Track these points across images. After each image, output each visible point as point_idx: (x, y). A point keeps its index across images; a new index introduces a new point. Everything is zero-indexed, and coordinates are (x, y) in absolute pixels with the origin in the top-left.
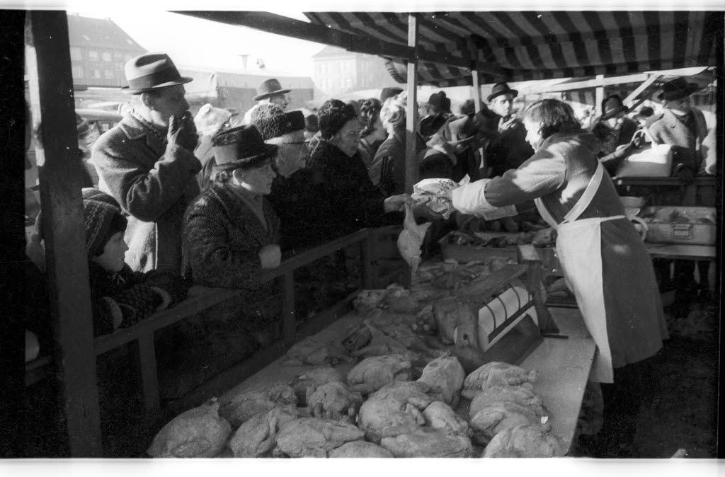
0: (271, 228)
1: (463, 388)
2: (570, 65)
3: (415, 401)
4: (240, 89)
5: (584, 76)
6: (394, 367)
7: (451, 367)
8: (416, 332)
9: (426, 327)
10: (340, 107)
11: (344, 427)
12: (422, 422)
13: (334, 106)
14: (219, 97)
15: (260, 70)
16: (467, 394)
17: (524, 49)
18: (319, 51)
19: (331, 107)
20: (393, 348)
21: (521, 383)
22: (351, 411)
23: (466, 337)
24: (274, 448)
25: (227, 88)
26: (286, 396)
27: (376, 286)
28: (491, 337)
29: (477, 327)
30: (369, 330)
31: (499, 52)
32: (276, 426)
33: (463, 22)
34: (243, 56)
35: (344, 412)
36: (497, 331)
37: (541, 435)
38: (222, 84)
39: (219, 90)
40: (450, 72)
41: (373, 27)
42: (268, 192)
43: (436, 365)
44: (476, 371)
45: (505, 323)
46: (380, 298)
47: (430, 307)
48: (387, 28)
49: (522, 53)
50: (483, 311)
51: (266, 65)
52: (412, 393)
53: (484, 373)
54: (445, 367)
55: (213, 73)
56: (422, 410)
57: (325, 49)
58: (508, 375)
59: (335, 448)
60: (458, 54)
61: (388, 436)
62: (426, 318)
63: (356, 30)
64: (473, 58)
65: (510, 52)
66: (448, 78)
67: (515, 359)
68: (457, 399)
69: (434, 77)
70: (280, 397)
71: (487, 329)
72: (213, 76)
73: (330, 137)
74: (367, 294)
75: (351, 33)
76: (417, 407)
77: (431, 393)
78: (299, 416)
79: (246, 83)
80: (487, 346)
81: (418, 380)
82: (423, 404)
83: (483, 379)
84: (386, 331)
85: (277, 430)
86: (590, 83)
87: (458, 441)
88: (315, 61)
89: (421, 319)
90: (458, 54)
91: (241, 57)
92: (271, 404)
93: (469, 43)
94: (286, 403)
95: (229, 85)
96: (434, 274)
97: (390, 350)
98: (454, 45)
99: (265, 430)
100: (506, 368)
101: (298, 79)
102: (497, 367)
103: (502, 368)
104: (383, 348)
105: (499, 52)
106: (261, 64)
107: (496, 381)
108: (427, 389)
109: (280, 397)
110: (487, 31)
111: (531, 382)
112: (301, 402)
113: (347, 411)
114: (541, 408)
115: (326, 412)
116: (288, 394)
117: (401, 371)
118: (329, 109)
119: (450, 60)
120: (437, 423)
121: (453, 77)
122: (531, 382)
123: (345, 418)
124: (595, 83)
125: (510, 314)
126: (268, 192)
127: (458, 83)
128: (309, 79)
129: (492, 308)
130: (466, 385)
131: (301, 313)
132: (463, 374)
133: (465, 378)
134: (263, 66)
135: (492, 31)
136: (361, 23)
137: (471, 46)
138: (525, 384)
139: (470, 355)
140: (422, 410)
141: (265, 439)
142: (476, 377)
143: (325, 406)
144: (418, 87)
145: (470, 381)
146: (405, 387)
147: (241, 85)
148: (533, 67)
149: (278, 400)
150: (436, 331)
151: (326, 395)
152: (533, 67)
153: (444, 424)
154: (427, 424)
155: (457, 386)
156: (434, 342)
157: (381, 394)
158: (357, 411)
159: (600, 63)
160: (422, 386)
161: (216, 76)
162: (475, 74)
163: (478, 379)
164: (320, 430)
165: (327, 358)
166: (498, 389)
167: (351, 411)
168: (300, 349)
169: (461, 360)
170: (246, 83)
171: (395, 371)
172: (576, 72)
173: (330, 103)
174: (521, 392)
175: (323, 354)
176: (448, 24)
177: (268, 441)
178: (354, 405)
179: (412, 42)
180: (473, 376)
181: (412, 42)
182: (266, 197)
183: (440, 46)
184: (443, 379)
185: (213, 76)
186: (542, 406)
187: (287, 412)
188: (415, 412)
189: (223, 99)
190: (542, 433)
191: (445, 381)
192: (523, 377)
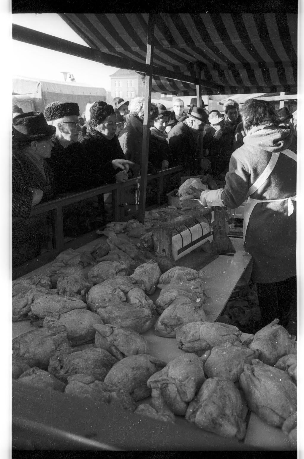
0: (49, 180)
1: (158, 282)
2: (260, 85)
3: (123, 287)
4: (57, 94)
5: (270, 92)
6: (117, 267)
7: (153, 269)
8: (139, 248)
9: (146, 245)
10: (103, 106)
11: (74, 300)
12: (125, 299)
13: (99, 106)
14: (43, 99)
15: (71, 81)
16: (159, 286)
17: (230, 72)
18: (113, 73)
19: (98, 106)
20: (122, 257)
21: (194, 279)
22: (83, 292)
23: (164, 251)
24: (29, 312)
25: (48, 93)
26: (43, 282)
27: (122, 220)
28: (179, 252)
29: (171, 245)
30: (109, 246)
31: (215, 74)
32: (33, 299)
33: (189, 52)
34: (64, 73)
35: (78, 293)
36: (184, 248)
37: (194, 309)
38: (45, 90)
39: (43, 93)
40: (184, 86)
41: (130, 52)
42: (49, 156)
43: (143, 267)
44: (167, 272)
45: (191, 243)
46: (123, 227)
47: (150, 233)
48: (139, 53)
49: (229, 75)
50: (176, 238)
51: (75, 78)
52: (123, 282)
53: (171, 273)
54: (148, 268)
55: (39, 82)
56: (126, 293)
57: (118, 71)
58: (187, 274)
59: (65, 313)
60: (188, 74)
61: (101, 307)
62: (146, 240)
63: (120, 53)
64: (197, 77)
65: (221, 74)
66: (183, 90)
67: (197, 267)
68: (154, 288)
69: (174, 88)
70: (39, 282)
71: (177, 246)
72: (39, 84)
73: (97, 126)
74: (113, 225)
75: (117, 55)
76: (123, 291)
77: (136, 283)
78: (47, 294)
79: (61, 91)
80: (177, 257)
81: (131, 276)
82: (127, 289)
83: (171, 277)
84: (120, 247)
85: (33, 301)
86: (276, 98)
87: (143, 311)
88: (112, 79)
89: (144, 239)
90: (188, 74)
91: (63, 74)
92: (33, 286)
93: (195, 66)
94: (42, 286)
95: (50, 91)
96: (161, 215)
97: (120, 258)
98: (186, 68)
99: (25, 301)
100: (185, 270)
101: (54, 85)
102: (179, 269)
103: (183, 270)
104: (115, 257)
105: (215, 74)
106: (72, 78)
107: (180, 278)
108: (134, 282)
109: (39, 282)
110: (204, 57)
111: (200, 278)
112: (53, 285)
113: (80, 292)
114: (202, 294)
115: (67, 292)
116: (45, 281)
117: (122, 270)
118: (96, 108)
119: (183, 77)
120: (133, 300)
121: (186, 90)
122: (200, 278)
123: (79, 296)
124: (279, 98)
125: (195, 239)
126: (49, 156)
127: (190, 93)
128: (104, 89)
129: (182, 235)
130: (161, 281)
131: (68, 232)
132: (160, 273)
133: (160, 276)
134: (73, 80)
135: (210, 60)
136: (107, 49)
137: (196, 68)
138: (197, 279)
139: (165, 262)
140: (126, 293)
141: (26, 306)
142: (167, 276)
143: (67, 289)
144: (152, 93)
145: (163, 278)
146: (120, 280)
147: (57, 91)
148: (236, 85)
149: (39, 284)
150: (152, 249)
151: (68, 282)
152: (236, 85)
153: (138, 301)
154: (127, 301)
155: (154, 280)
156: (150, 255)
157: (105, 283)
158: (87, 292)
159: (280, 84)
160: (131, 279)
161: (40, 83)
162: (198, 87)
163: (168, 277)
164: (59, 302)
165: (80, 262)
166: (177, 283)
167: (83, 292)
168: (63, 256)
169: (159, 265)
170: (61, 91)
171: (117, 270)
172: (265, 89)
173: (97, 104)
174: (192, 285)
175: (78, 259)
176: (179, 52)
177: (27, 308)
178: (85, 289)
179: (148, 62)
180: (165, 276)
181: (148, 62)
182: (46, 159)
183: (176, 67)
184: (146, 276)
185: (39, 84)
186: (204, 293)
187: (41, 291)
188: (121, 293)
189: (46, 100)
190: (195, 307)
191: (147, 277)
192: (196, 275)
